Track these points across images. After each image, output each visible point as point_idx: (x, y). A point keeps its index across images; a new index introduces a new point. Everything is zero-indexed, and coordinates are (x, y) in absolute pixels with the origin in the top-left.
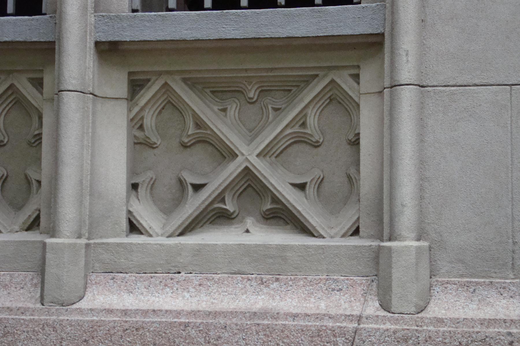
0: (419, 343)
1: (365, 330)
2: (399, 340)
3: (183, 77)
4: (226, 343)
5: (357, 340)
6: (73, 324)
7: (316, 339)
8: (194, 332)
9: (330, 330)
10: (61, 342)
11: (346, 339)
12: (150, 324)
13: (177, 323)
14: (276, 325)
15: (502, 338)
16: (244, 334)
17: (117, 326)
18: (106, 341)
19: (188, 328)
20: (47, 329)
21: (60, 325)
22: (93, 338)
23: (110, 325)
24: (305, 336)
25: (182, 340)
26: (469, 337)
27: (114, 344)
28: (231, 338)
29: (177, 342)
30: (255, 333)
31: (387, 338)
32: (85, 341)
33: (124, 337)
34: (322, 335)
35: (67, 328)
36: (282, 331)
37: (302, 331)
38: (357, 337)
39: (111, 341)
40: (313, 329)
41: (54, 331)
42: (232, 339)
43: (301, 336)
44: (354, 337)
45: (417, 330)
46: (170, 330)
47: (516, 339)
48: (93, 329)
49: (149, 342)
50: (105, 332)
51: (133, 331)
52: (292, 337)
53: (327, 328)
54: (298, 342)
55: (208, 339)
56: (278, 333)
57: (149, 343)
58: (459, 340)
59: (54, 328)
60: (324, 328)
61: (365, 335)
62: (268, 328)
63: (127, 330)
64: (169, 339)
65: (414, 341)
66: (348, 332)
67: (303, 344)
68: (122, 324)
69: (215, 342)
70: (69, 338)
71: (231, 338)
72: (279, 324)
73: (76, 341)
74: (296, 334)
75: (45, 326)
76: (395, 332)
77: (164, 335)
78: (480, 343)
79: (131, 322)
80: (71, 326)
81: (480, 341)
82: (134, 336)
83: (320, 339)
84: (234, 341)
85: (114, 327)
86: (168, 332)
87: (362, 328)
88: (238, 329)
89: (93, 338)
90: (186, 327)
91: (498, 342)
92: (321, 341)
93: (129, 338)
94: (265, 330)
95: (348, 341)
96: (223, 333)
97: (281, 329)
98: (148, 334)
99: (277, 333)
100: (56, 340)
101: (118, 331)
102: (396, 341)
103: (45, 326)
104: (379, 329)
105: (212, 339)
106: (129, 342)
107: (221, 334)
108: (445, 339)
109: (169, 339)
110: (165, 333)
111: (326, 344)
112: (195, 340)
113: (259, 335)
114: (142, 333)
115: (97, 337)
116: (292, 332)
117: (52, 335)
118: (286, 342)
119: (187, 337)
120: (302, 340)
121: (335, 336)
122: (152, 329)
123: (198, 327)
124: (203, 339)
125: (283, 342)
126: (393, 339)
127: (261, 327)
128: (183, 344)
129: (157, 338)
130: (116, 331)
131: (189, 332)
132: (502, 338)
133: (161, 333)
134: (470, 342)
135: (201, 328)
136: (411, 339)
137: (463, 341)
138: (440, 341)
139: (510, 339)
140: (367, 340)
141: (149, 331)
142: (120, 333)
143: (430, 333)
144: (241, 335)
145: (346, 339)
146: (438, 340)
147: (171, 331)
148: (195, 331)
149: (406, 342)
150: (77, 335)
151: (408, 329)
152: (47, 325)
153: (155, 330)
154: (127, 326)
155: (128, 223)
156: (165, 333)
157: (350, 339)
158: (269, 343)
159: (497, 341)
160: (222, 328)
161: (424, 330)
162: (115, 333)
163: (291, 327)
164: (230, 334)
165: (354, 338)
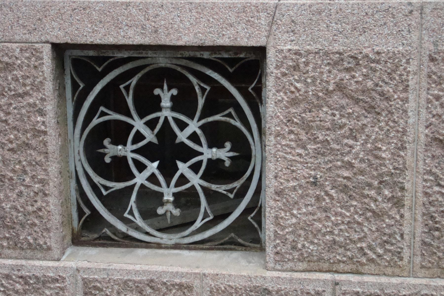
0: (331, 15)
1: (284, 5)
2: (314, 13)
3: (160, 188)
4: (163, 20)
5: (277, 14)
6: (27, 4)
7: (242, 14)
8: (135, 11)
9: (254, 6)
10: (18, 21)
11: (268, 14)
12: (95, 4)
13: (119, 3)
14: (207, 3)
15: (403, 7)
16: (179, 12)
17: (66, 6)
18: (58, 20)
19: (129, 7)
20: (4, 9)
21: (16, 5)
22: (46, 17)
23: (60, 5)
24: (232, 13)
25: (124, 18)
26: (375, 7)
27: (64, 22)
28: (168, 15)
29: (120, 20)
30: (188, 11)
31: (303, 12)
32: (39, 19)
33: (73, 16)
34: (247, 11)
35: (23, 8)
36: (212, 9)
37: (230, 8)
38: (277, 12)
39: (62, 19)
40: (239, 6)
41: (11, 11)
42: (168, 17)
43: (229, 12)
44: (275, 12)
45: (329, 4)
46: (114, 9)
47: (415, 8)
48: (45, 9)
49: (95, 19)
50: (56, 11)
51: (81, 10)
52: (221, 14)
53: (251, 5)
54: (226, 18)
55: (147, 16)
56: (209, 11)
57: (96, 21)
58: (366, 11)
59: (11, 8)
60: (249, 5)
61: (285, 9)
62: (200, 6)
63: (75, 9)
64: (113, 17)
65: (327, 13)
66: (270, 7)
67: (230, 19)
68: (71, 4)
69: (153, 20)
70: (25, 17)
71: (168, 15)
72: (209, 3)
73: (31, 20)
74: (224, 11)
75: (3, 7)
76: (310, 6)
77: (108, 13)
78: (384, 13)
79: (79, 2)
80: (26, 6)
81: (384, 11)
82: (82, 14)
83: (245, 15)
84: (170, 18)
85: (64, 7)
86: (111, 11)
87: (282, 4)
88: (173, 8)
89: (46, 17)
90: (127, 6)
91: (400, 12)
92: (246, 16)
93: (78, 16)
94: (197, 8)
95: (269, 16)
96: (160, 11)
97: (211, 6)
98: (94, 13)
99: (207, 10)
100: (13, 19)
101: (67, 10)
102: (311, 14)
103: (3, 7)
104: (296, 4)
105: (151, 17)
106: (78, 20)
107: (158, 12)
108: (354, 10)
109: (113, 17)
110: (109, 12)
111: (250, 18)
112: (136, 18)
113: (192, 12)
114: (89, 12)
115: (49, 15)
116: (221, 9)
117: (9, 15)
118: (216, 18)
119: (129, 15)
120: (229, 16)
121: (258, 12)
122: (97, 8)
123: (138, 6)
124: (143, 17)
125: (213, 18)
126: (308, 13)
127: (194, 5)
128: (126, 21)
129: (102, 17)
130: (65, 10)
131: (130, 11)
132: (403, 7)
133: (106, 12)
134: (375, 12)
135: (141, 7)
136: (324, 11)
137: (369, 12)
138: (349, 12)
139: (410, 8)
140: (286, 14)
141: (94, 10)
142: (69, 12)
143: (341, 6)
144: (176, 13)
145: (268, 14)
146: (348, 11)
147: (114, 10)
148: (136, 10)
149: (320, 14)
150: (32, 14)
151: (322, 3)
152: (5, 6)
153: (100, 10)
154: (75, 6)
155: (84, 172)
156: (109, 12)
157: (272, 13)
158: (201, 19)
159: (398, 11)
160: (159, 7)
161: (335, 3)
162: (65, 12)
163: (220, 5)
164: (166, 12)
165: (275, 13)
